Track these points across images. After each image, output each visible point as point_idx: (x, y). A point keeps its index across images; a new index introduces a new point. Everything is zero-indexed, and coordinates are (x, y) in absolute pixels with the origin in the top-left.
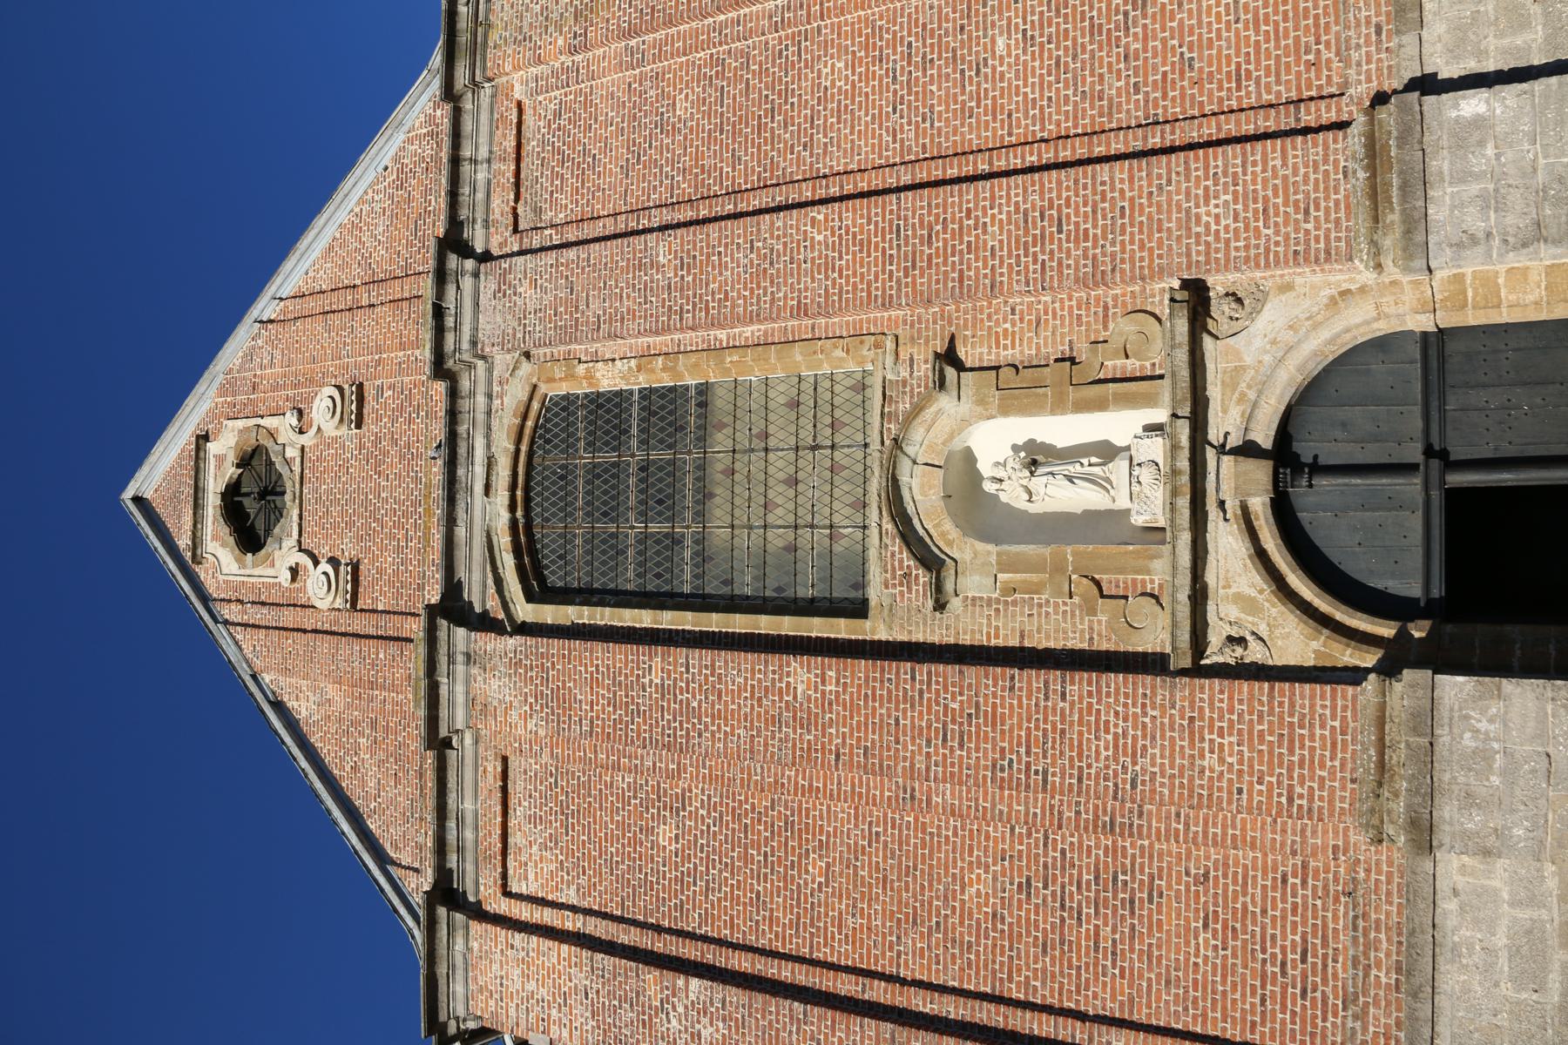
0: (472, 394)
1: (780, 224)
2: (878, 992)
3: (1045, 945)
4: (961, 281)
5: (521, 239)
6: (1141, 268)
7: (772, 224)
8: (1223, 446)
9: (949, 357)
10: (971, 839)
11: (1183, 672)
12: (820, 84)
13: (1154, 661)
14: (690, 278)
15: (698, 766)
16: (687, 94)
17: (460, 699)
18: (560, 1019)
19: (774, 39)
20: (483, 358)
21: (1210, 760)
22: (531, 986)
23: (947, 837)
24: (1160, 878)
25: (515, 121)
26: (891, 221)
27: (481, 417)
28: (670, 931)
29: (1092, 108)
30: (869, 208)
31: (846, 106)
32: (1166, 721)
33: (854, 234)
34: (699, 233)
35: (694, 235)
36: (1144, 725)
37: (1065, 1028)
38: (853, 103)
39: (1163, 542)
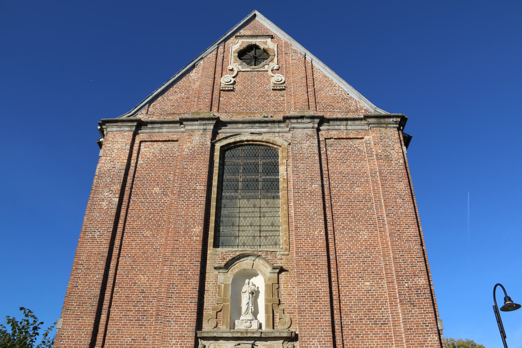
0: (279, 127)
1: (321, 221)
2: (115, 251)
3: (128, 297)
4: (301, 274)
5: (323, 141)
6: (302, 324)
7: (321, 219)
8: (254, 345)
9: (282, 270)
10: (155, 277)
11: (196, 334)
12: (361, 231)
13: (200, 326)
14: (307, 195)
15: (175, 199)
16: (361, 191)
17: (194, 127)
18: (107, 160)
19: (375, 217)
20: (290, 131)
21: (174, 341)
22: (116, 151)
23: (156, 270)
24: (145, 328)
25: (358, 137)
26: (319, 254)
27: (273, 130)
28: (131, 191)
29: (347, 310)
30: (323, 247)
31: (354, 239)
32: (184, 330)
33: (316, 243)
34: (320, 197)
35: (320, 196)
36: (183, 324)
37: (107, 303)
38: (354, 241)
39: (230, 329)
